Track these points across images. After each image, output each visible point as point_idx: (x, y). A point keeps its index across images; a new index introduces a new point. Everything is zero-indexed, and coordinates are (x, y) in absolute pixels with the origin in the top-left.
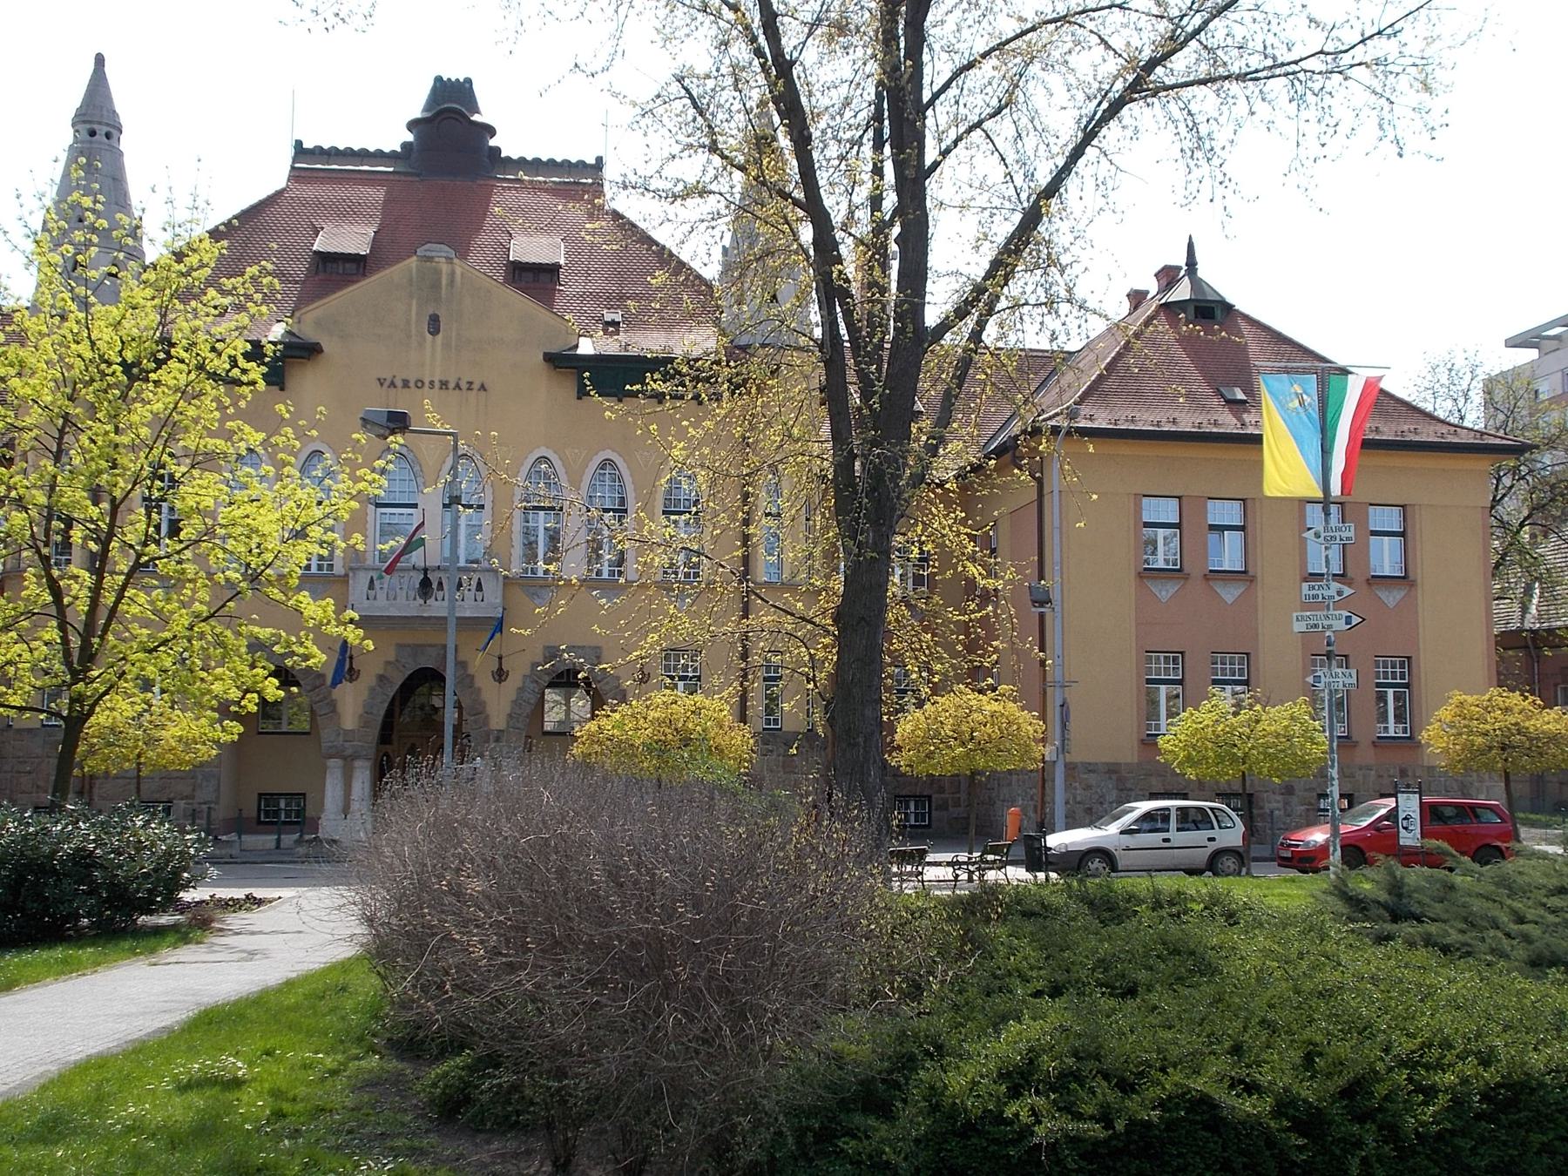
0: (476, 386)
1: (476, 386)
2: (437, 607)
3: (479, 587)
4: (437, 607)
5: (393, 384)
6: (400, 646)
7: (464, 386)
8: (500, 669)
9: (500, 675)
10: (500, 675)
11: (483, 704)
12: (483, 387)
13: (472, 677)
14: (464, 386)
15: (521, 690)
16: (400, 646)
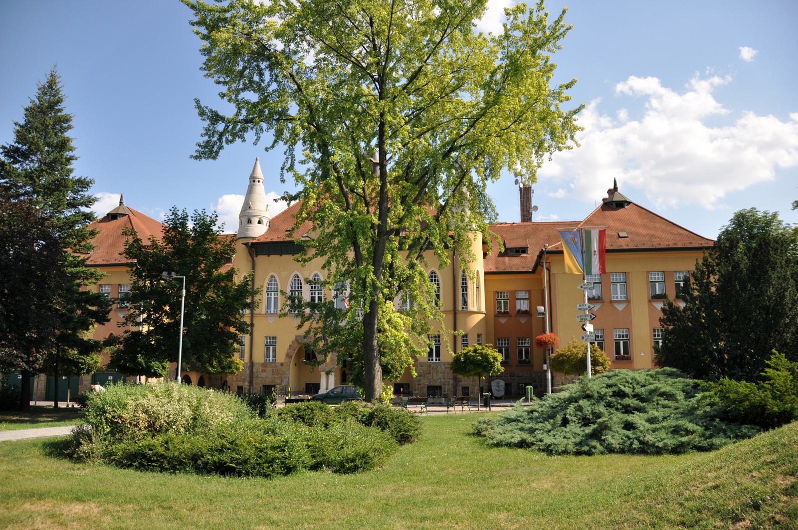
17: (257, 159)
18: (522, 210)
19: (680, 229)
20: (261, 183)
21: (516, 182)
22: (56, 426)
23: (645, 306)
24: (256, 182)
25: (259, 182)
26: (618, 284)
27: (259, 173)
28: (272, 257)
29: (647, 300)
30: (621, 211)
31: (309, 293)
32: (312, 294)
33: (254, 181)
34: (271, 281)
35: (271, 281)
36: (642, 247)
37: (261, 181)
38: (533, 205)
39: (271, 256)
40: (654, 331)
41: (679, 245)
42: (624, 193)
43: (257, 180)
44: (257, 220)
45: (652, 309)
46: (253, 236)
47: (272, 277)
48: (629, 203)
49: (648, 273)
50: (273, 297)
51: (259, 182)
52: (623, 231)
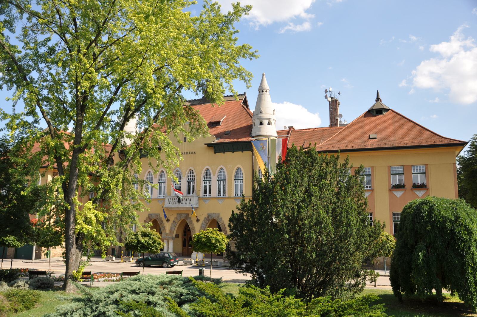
0: (193, 153)
1: (193, 153)
2: (183, 205)
3: (190, 200)
4: (183, 205)
5: (189, 153)
6: (178, 214)
7: (191, 153)
8: (198, 219)
9: (198, 221)
10: (198, 221)
11: (194, 227)
12: (195, 153)
13: (192, 221)
14: (191, 153)
15: (202, 224)
16: (178, 214)
17: (263, 75)
18: (331, 118)
19: (427, 132)
20: (268, 93)
21: (326, 97)
22: (33, 269)
23: (387, 193)
24: (264, 92)
25: (266, 92)
26: (419, 175)
27: (266, 85)
28: (226, 153)
29: (388, 189)
30: (380, 117)
31: (216, 182)
32: (204, 183)
33: (263, 91)
34: (221, 172)
35: (221, 172)
36: (425, 144)
37: (268, 91)
38: (338, 114)
39: (235, 153)
40: (394, 215)
41: (416, 144)
42: (386, 103)
43: (264, 91)
44: (267, 121)
45: (392, 197)
46: (264, 134)
47: (239, 168)
48: (387, 110)
49: (389, 167)
50: (222, 184)
51: (266, 92)
52: (374, 133)
